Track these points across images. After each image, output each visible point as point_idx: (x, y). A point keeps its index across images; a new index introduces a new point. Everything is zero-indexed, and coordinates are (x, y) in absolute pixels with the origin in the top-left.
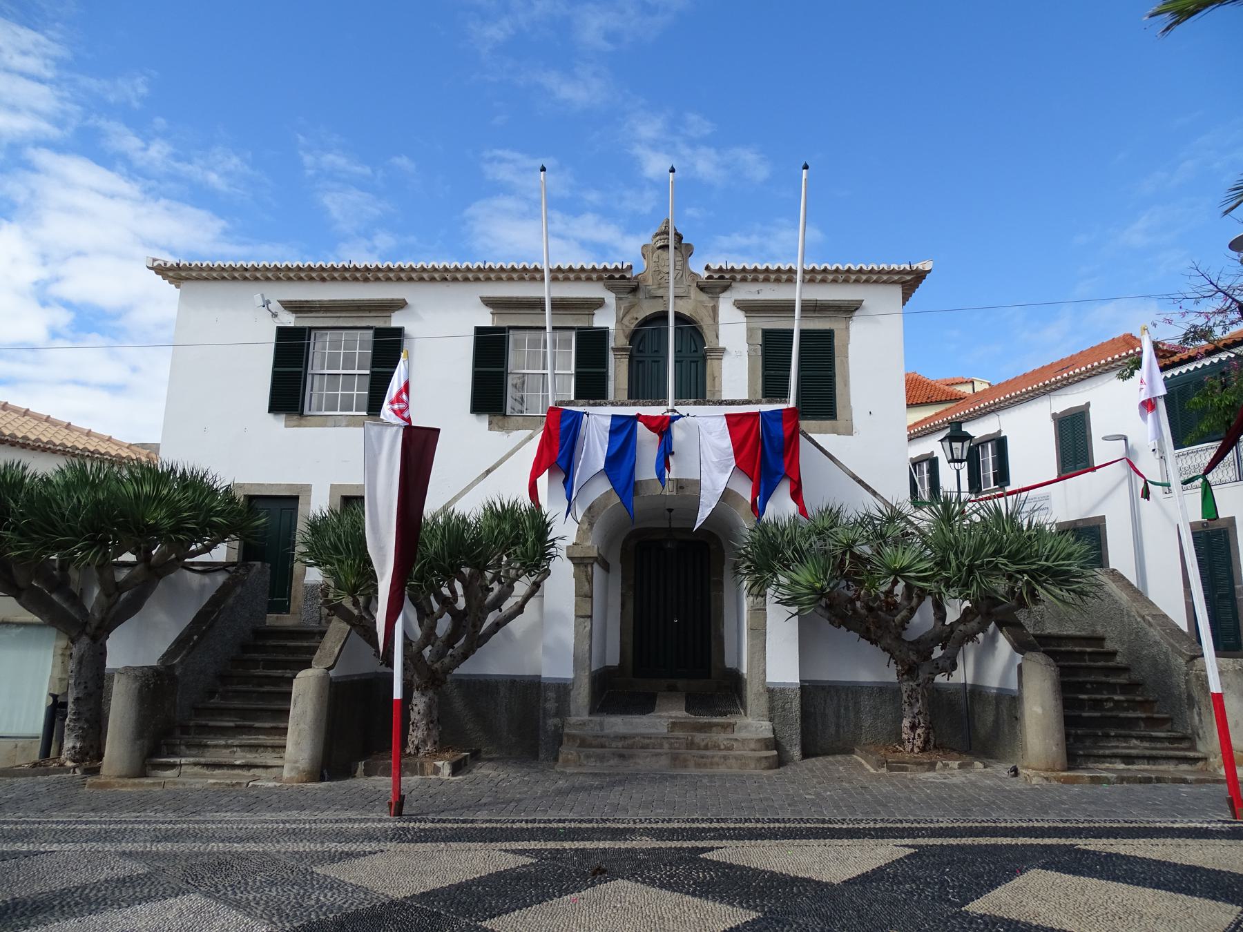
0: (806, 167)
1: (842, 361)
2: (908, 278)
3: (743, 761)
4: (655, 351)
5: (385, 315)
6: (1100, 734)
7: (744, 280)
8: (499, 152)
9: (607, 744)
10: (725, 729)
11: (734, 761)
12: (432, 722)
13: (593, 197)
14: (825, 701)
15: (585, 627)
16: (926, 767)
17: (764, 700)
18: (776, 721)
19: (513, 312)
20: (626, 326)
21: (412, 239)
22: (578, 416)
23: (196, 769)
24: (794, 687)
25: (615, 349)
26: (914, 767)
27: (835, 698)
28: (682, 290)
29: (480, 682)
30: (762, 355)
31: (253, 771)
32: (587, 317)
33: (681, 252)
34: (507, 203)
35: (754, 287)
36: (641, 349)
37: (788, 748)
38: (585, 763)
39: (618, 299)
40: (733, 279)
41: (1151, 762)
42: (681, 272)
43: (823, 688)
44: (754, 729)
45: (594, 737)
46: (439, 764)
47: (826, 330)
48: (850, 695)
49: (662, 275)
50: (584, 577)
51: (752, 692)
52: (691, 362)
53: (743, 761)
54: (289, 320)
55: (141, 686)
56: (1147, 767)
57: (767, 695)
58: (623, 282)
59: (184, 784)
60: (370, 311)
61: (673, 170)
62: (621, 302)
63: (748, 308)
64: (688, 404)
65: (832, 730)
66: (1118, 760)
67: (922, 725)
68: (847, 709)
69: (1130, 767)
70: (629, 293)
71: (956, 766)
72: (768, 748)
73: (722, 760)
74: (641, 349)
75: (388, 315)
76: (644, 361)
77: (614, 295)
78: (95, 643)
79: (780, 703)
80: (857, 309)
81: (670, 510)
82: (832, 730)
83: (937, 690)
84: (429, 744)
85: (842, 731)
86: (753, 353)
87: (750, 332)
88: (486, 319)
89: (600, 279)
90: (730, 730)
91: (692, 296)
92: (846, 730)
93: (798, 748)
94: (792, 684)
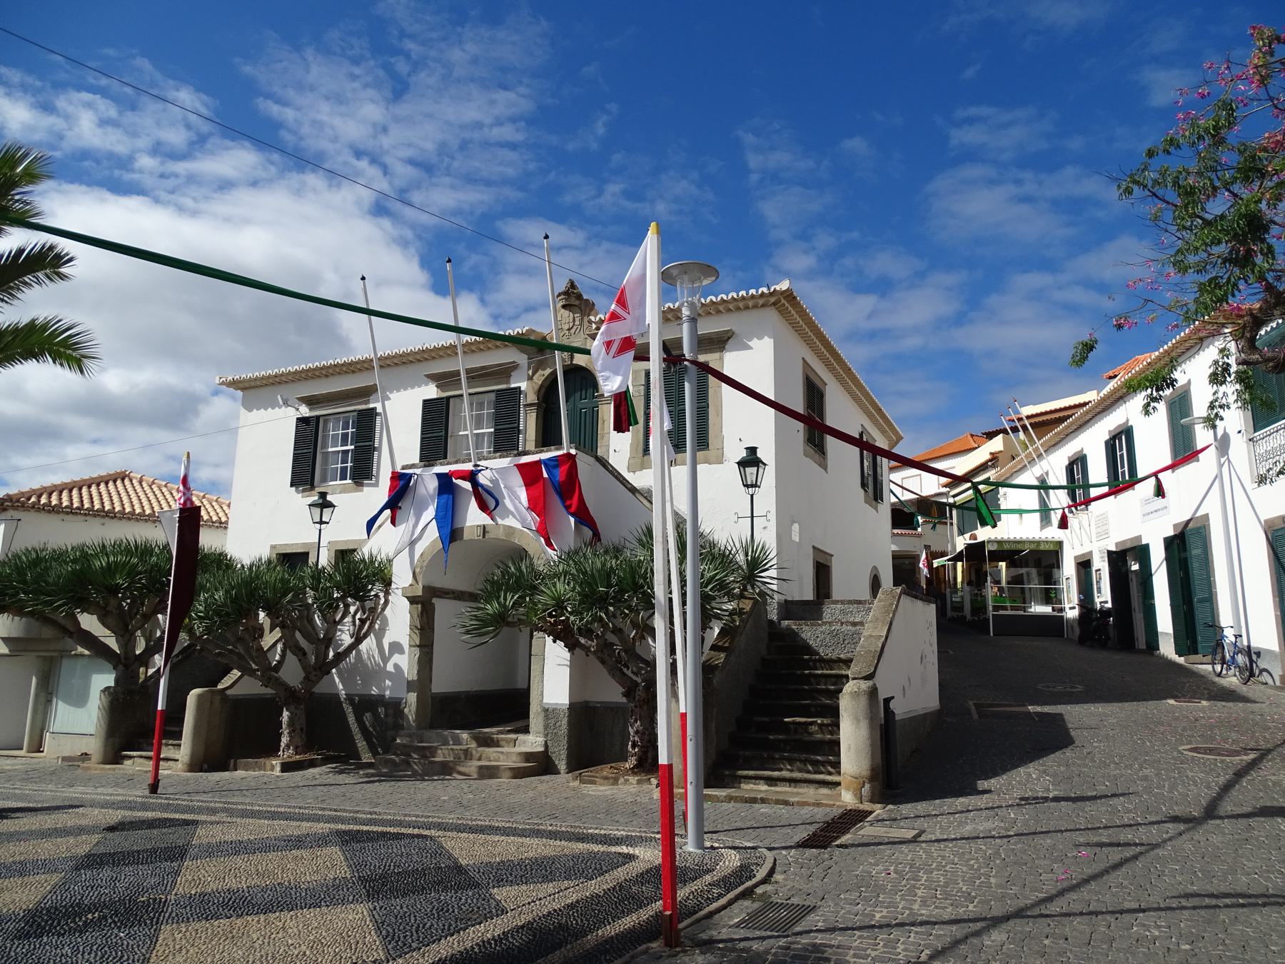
0: (449, 261)
1: (715, 391)
6: (765, 756)
8: (973, 111)
13: (1076, 144)
16: (611, 781)
21: (855, 235)
23: (142, 760)
24: (563, 707)
25: (526, 406)
31: (169, 762)
34: (974, 171)
37: (557, 762)
41: (792, 784)
51: (534, 709)
54: (305, 411)
56: (788, 789)
57: (542, 714)
61: (546, 237)
64: (495, 458)
66: (762, 782)
69: (772, 788)
71: (635, 782)
72: (527, 761)
77: (526, 356)
80: (729, 338)
88: (431, 391)
93: (564, 762)
94: (562, 704)
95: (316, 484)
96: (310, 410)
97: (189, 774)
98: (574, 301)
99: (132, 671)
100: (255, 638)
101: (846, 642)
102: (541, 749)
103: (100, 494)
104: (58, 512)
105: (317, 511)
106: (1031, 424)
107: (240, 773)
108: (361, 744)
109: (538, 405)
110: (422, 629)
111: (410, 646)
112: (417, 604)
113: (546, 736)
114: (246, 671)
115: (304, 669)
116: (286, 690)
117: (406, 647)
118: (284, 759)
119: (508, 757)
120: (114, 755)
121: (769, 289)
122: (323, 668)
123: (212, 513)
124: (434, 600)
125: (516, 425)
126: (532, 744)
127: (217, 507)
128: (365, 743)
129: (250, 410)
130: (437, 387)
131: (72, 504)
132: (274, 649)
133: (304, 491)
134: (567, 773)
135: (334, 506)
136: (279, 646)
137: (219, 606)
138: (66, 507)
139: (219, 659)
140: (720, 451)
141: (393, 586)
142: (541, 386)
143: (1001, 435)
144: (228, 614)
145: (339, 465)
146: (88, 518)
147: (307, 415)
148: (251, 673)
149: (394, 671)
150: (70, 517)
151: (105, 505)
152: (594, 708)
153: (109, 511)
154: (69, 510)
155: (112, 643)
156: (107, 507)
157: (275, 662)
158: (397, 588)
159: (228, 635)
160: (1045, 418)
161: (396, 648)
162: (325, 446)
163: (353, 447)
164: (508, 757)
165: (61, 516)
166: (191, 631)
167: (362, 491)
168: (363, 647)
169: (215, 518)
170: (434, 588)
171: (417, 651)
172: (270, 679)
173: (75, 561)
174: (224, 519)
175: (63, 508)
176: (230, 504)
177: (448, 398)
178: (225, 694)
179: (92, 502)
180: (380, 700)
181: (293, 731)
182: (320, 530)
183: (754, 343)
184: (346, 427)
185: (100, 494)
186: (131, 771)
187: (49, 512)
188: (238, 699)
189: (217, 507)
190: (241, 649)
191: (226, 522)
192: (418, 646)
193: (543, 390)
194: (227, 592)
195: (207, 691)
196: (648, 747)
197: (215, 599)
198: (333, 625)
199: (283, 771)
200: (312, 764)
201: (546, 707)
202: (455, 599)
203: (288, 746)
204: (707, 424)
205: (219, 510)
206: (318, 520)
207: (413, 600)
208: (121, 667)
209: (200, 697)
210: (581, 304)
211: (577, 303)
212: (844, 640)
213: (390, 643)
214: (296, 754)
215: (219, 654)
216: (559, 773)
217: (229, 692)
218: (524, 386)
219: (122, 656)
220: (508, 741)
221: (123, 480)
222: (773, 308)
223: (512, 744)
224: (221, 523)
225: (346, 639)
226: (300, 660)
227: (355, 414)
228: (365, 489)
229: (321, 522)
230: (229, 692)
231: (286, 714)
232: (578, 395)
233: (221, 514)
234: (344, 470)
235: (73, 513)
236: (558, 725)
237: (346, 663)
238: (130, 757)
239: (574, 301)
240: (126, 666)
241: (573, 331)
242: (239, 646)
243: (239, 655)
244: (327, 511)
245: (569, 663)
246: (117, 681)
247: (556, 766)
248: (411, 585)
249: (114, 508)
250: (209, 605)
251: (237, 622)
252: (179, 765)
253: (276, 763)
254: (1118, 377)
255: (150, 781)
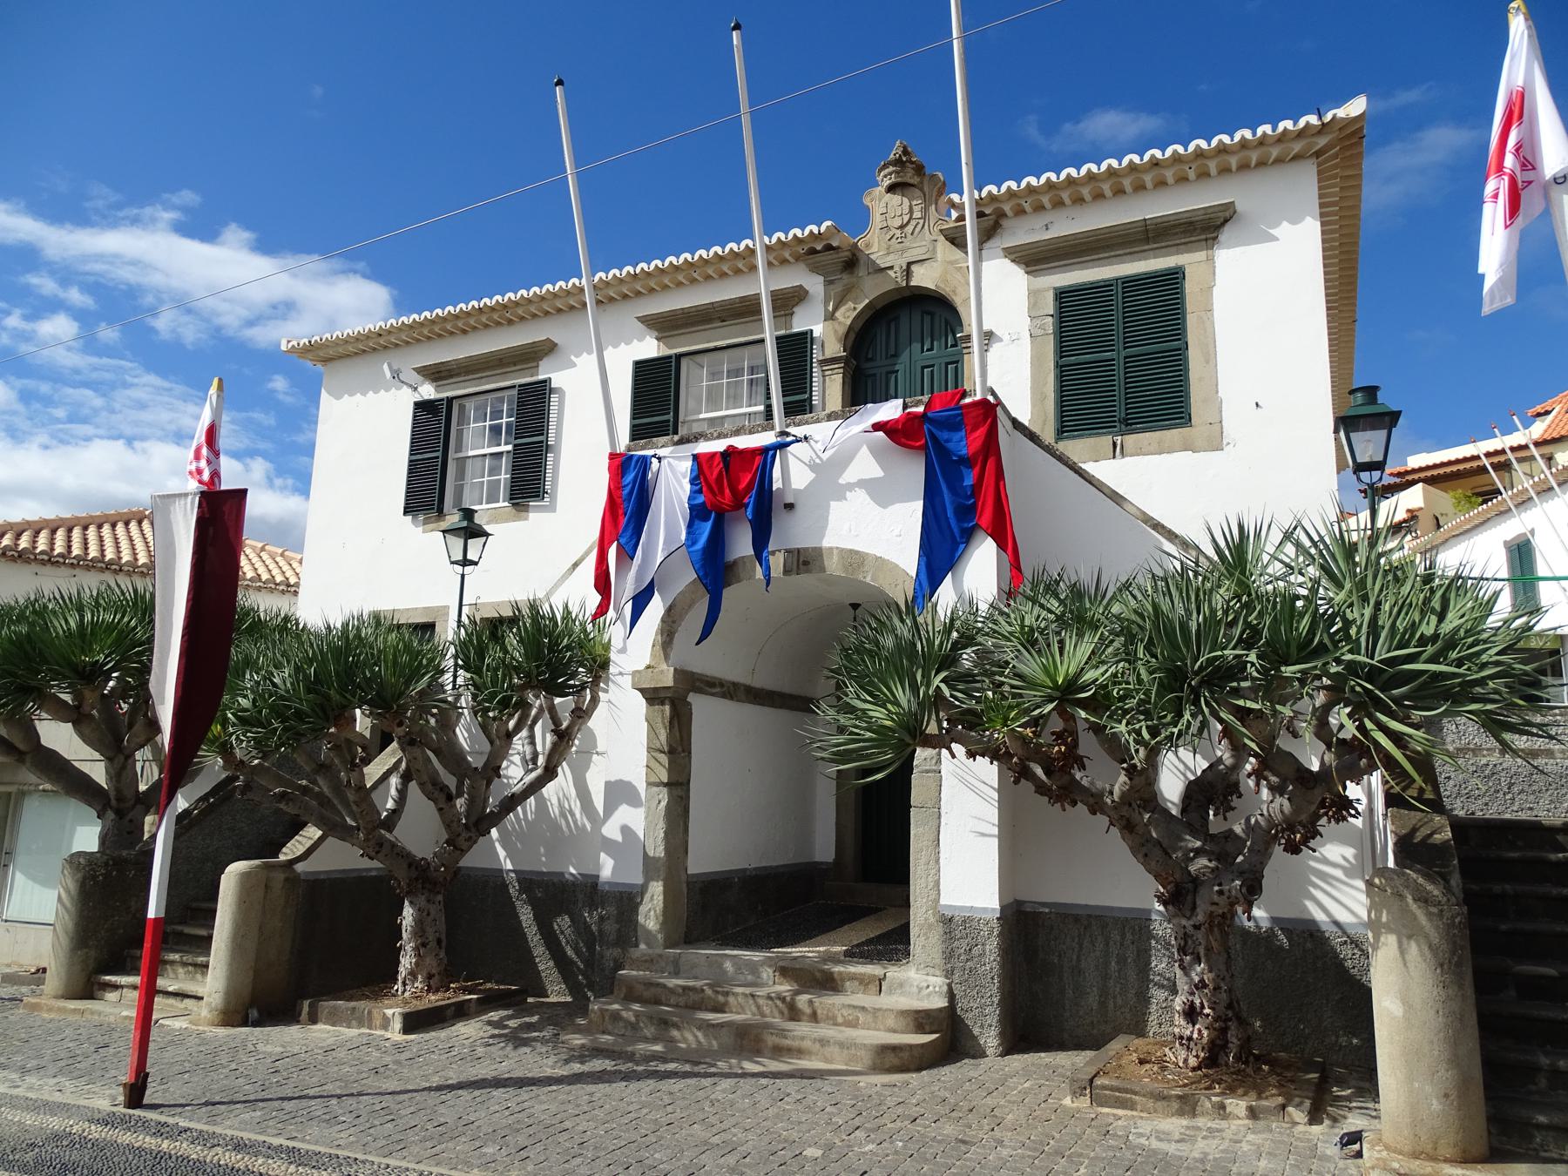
2: (1322, 142)
3: (853, 1052)
4: (893, 356)
5: (529, 365)
7: (1020, 212)
9: (663, 999)
10: (867, 984)
11: (836, 1049)
12: (424, 945)
14: (1081, 945)
15: (660, 802)
17: (936, 937)
18: (956, 977)
19: (700, 328)
20: (840, 323)
22: (644, 463)
24: (988, 916)
26: (1150, 1104)
27: (1100, 938)
28: (924, 250)
29: (554, 884)
30: (1054, 333)
31: (188, 1002)
32: (784, 318)
33: (922, 190)
35: (1038, 221)
36: (870, 356)
37: (976, 1031)
38: (610, 1027)
39: (828, 283)
40: (1001, 215)
42: (921, 221)
43: (1077, 919)
44: (915, 990)
45: (645, 984)
46: (389, 1012)
47: (1169, 269)
48: (1129, 936)
49: (891, 233)
50: (660, 720)
51: (920, 915)
52: (947, 364)
53: (853, 1052)
54: (428, 391)
55: (84, 878)
57: (940, 929)
58: (829, 257)
59: (100, 1014)
60: (515, 365)
62: (832, 287)
63: (1033, 259)
65: (1092, 1000)
67: (1207, 1011)
68: (1122, 961)
70: (842, 273)
72: (920, 1028)
73: (818, 1045)
74: (870, 356)
75: (534, 364)
76: (875, 375)
77: (822, 279)
78: (121, 818)
79: (964, 944)
80: (1226, 221)
81: (855, 606)
82: (1092, 1000)
83: (1311, 935)
84: (420, 979)
85: (1111, 1005)
86: (1040, 332)
87: (1034, 294)
88: (650, 348)
89: (798, 258)
90: (874, 988)
91: (939, 255)
92: (1119, 1001)
93: (994, 1032)
94: (985, 909)
95: (445, 510)
96: (437, 389)
97: (222, 1032)
98: (910, 177)
99: (131, 821)
100: (354, 765)
101: (1516, 789)
102: (940, 1002)
103: (101, 539)
104: (28, 561)
105: (457, 543)
106: (1492, 464)
107: (322, 1032)
108: (545, 965)
109: (846, 361)
110: (671, 752)
111: (649, 784)
112: (663, 703)
113: (949, 974)
114: (333, 828)
115: (448, 826)
116: (410, 865)
117: (641, 787)
118: (406, 1002)
119: (875, 1017)
120: (87, 987)
121: (1320, 118)
122: (481, 823)
123: (275, 572)
124: (692, 698)
125: (806, 396)
126: (920, 989)
127: (282, 563)
128: (551, 963)
129: (338, 397)
130: (658, 339)
131: (52, 549)
132: (381, 787)
133: (426, 522)
134: (1002, 1055)
135: (487, 535)
136: (394, 781)
137: (282, 698)
138: (42, 552)
139: (282, 806)
140: (1216, 427)
141: (613, 669)
142: (850, 328)
143: (1420, 485)
144: (299, 715)
145: (485, 479)
146: (77, 572)
147: (432, 397)
148: (344, 833)
149: (620, 839)
150: (48, 569)
151: (106, 553)
152: (1036, 916)
153: (111, 562)
154: (46, 557)
155: (98, 772)
156: (110, 554)
157: (385, 813)
158: (621, 674)
159: (300, 759)
160: (1448, 470)
161: (619, 792)
162: (459, 449)
163: (510, 447)
164: (875, 1017)
165: (34, 567)
166: (225, 750)
167: (526, 519)
168: (549, 790)
169: (279, 579)
170: (693, 674)
171: (663, 795)
172: (381, 845)
173: (22, 617)
174: (293, 580)
175: (35, 555)
176: (301, 559)
177: (679, 357)
178: (294, 871)
179: (86, 549)
180: (590, 889)
181: (424, 945)
182: (463, 576)
183: (1284, 230)
184: (497, 414)
185: (101, 539)
186: (112, 1019)
187: (13, 559)
188: (315, 881)
189: (282, 563)
190: (323, 786)
191: (297, 585)
192: (665, 785)
193: (852, 336)
194: (298, 669)
195: (257, 867)
196: (1227, 1020)
197: (274, 685)
198: (500, 742)
199: (407, 1030)
200: (460, 1012)
201: (949, 913)
202: (723, 696)
203: (413, 974)
204: (1187, 379)
205: (286, 568)
206: (461, 558)
207: (653, 696)
208: (110, 815)
209: (245, 877)
210: (922, 182)
211: (916, 180)
212: (1510, 785)
213: (608, 784)
214: (428, 991)
215: (283, 795)
216: (983, 1055)
217: (300, 867)
218: (818, 330)
219: (112, 794)
220: (864, 981)
221: (140, 523)
222: (1314, 160)
223: (874, 988)
224: (289, 585)
225: (514, 773)
226: (440, 810)
227: (515, 392)
228: (532, 515)
229: (465, 562)
230: (300, 867)
231: (408, 915)
232: (916, 346)
233: (289, 573)
234: (494, 486)
235: (53, 563)
236: (975, 951)
237: (517, 816)
238: (116, 987)
239: (910, 177)
240: (120, 813)
241: (909, 229)
242: (320, 781)
243: (320, 797)
244: (474, 545)
245: (995, 831)
246: (103, 839)
247: (975, 1038)
248: (648, 667)
249: (120, 558)
250: (262, 696)
251: (318, 732)
252: (204, 1011)
253: (393, 1013)
254: (1554, 413)
255: (126, 1077)
